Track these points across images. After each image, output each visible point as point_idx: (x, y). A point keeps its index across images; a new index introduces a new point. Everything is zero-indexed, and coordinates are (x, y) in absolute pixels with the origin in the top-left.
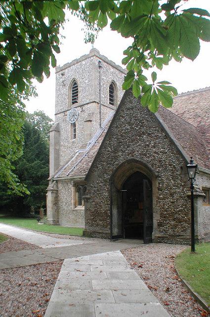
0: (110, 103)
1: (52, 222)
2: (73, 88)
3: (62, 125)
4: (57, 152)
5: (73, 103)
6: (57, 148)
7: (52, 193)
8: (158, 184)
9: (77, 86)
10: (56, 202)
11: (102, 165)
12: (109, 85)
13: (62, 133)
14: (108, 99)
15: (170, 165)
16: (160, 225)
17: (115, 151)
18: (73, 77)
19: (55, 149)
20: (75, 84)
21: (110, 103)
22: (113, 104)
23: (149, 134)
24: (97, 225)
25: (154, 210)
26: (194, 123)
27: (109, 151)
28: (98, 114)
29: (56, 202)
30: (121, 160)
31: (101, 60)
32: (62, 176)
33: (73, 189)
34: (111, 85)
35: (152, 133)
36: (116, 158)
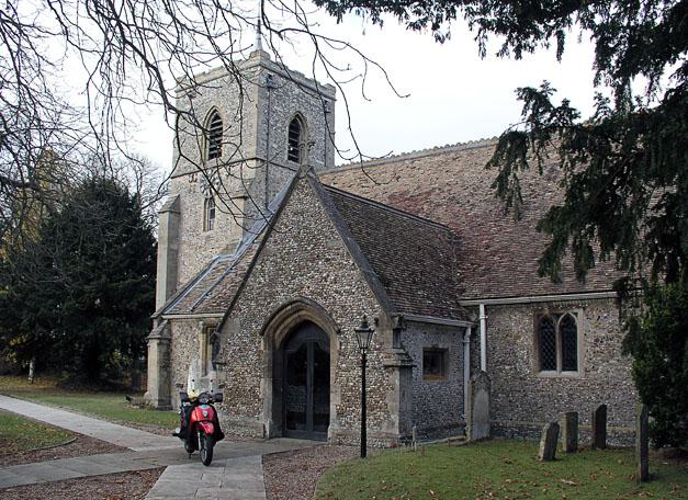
0: (290, 158)
1: (157, 403)
2: (213, 126)
3: (187, 201)
4: (174, 256)
5: (211, 157)
6: (174, 247)
7: (158, 344)
8: (338, 345)
9: (221, 123)
10: (166, 364)
11: (249, 306)
12: (288, 123)
13: (186, 215)
14: (287, 134)
15: (360, 314)
16: (340, 414)
17: (272, 283)
18: (213, 103)
19: (169, 250)
20: (217, 117)
21: (290, 158)
22: (296, 160)
23: (328, 260)
24: (237, 413)
25: (332, 389)
26: (442, 215)
27: (260, 283)
28: (263, 183)
29: (166, 364)
30: (281, 300)
31: (272, 74)
32: (181, 311)
33: (201, 338)
34: (294, 121)
35: (333, 259)
36: (272, 295)
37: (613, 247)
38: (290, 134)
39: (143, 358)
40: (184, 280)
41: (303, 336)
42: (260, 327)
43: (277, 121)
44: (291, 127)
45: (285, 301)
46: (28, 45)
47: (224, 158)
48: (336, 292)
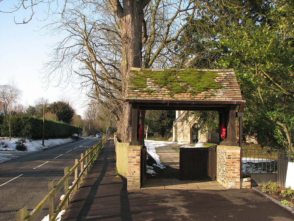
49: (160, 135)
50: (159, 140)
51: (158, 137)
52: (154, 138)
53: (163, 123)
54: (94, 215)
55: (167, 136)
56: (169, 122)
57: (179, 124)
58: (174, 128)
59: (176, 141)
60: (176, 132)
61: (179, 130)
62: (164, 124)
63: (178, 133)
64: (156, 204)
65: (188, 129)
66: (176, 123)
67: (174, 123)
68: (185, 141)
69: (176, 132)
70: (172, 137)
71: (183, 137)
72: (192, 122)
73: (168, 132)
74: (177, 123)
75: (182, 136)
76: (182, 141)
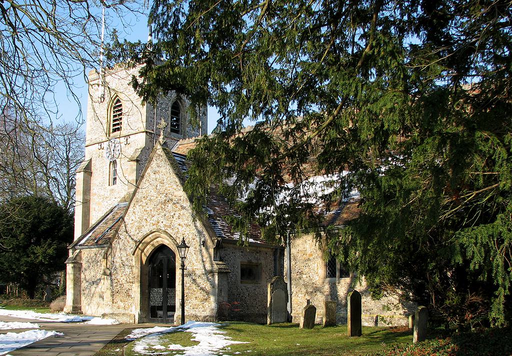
2: (115, 108)
5: (114, 130)
12: (170, 104)
14: (169, 112)
20: (118, 101)
37: (341, 171)
38: (172, 113)
39: (422, 278)
40: (93, 221)
41: (161, 256)
42: (132, 250)
43: (162, 104)
44: (173, 107)
45: (148, 232)
46: (13, 59)
47: (124, 132)
48: (179, 225)
49: (24, 292)
50: (21, 304)
51: (19, 297)
52: (5, 301)
53: (34, 253)
54: (47, 342)
55: (43, 295)
56: (50, 251)
57: (87, 254)
58: (69, 267)
59: (76, 310)
60: (77, 281)
61: (88, 275)
62: (37, 257)
63: (84, 285)
64: (270, 304)
65: (132, 267)
66: (78, 251)
67: (71, 251)
68: (122, 311)
69: (77, 281)
70: (62, 297)
71: (113, 296)
72: (147, 239)
73: (46, 284)
74: (80, 252)
75: (108, 295)
76: (108, 310)
